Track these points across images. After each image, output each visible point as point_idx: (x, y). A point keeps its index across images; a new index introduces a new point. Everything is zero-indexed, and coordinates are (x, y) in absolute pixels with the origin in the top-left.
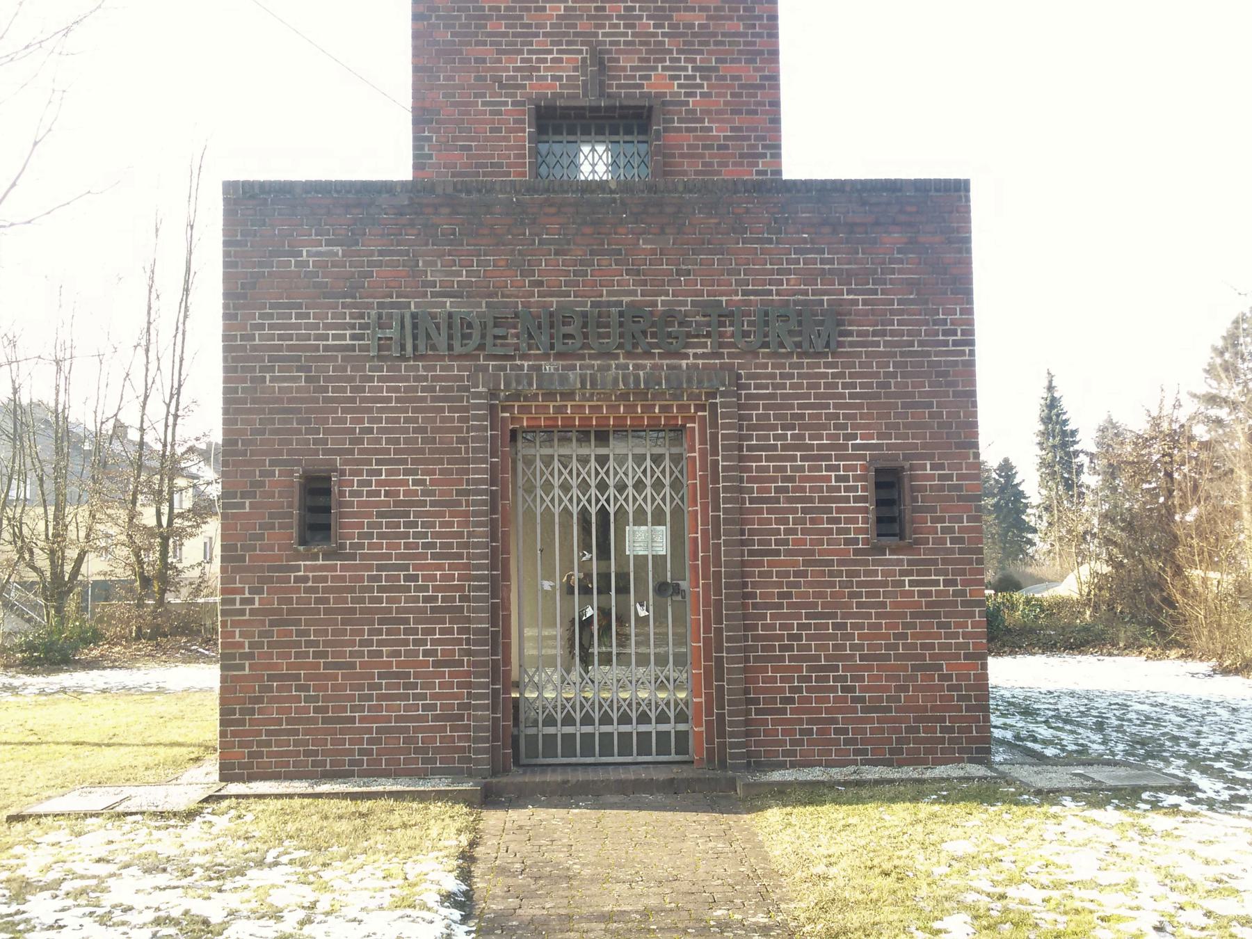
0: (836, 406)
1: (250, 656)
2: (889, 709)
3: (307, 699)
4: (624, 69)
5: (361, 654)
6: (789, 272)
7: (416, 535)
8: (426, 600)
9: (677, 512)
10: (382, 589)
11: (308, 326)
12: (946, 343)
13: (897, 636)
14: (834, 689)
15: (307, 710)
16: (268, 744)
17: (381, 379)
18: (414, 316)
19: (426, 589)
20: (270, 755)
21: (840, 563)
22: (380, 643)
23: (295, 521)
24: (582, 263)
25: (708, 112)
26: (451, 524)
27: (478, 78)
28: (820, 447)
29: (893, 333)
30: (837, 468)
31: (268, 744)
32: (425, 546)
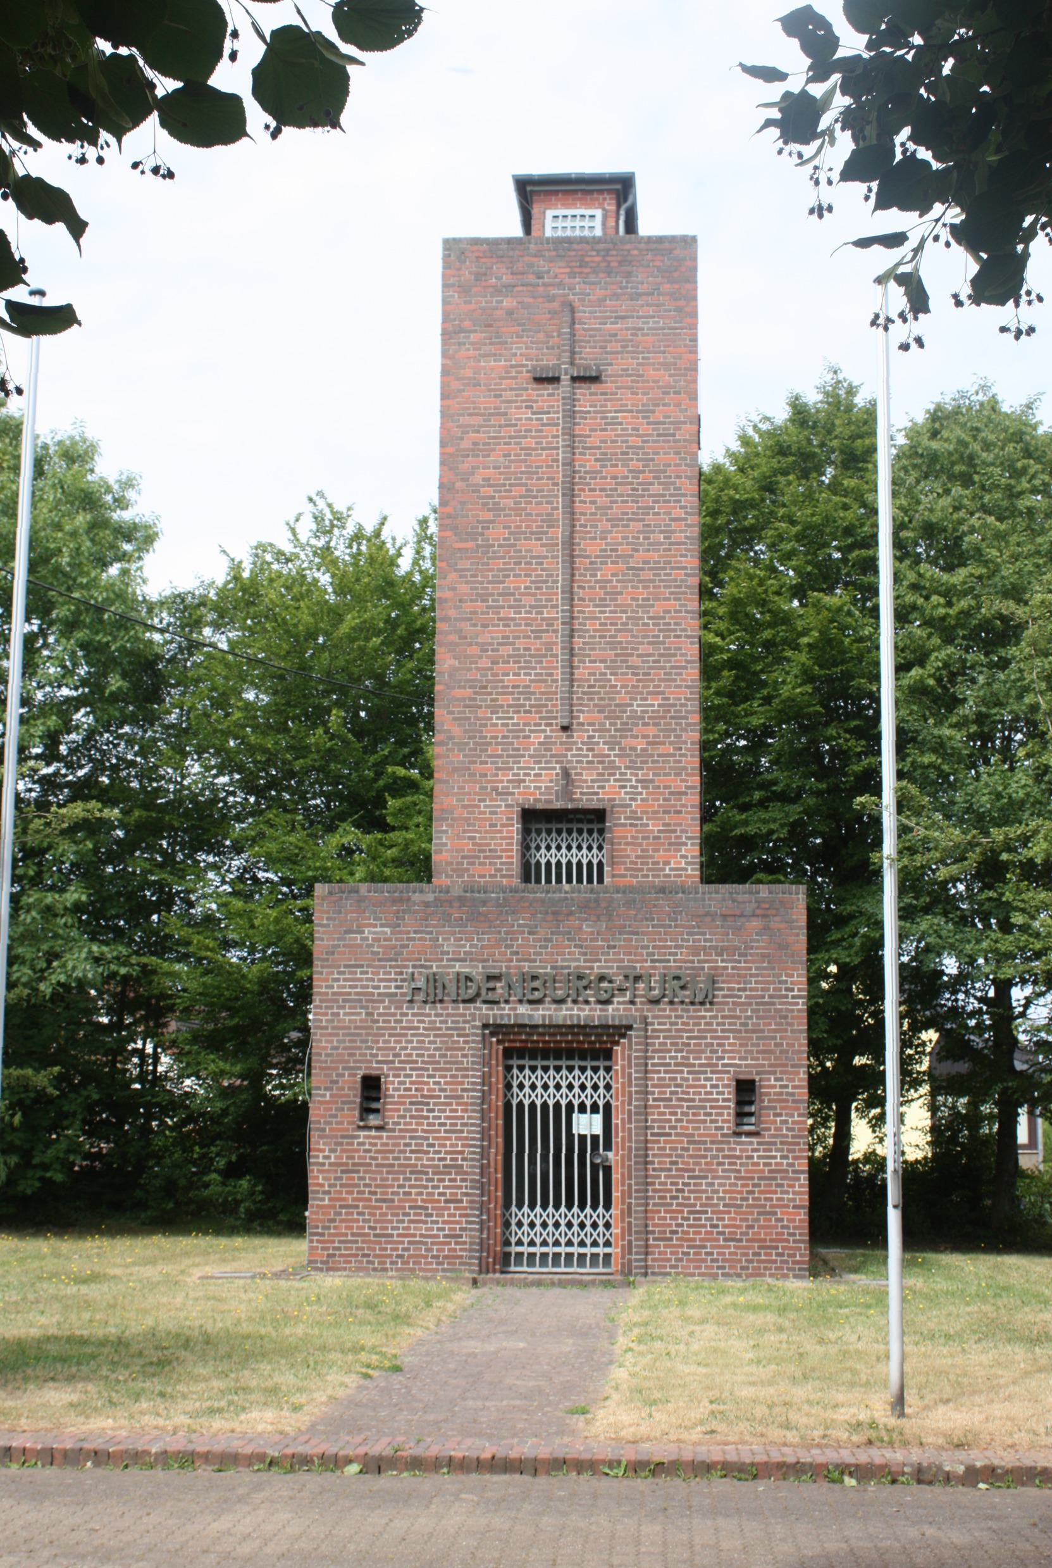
0: (712, 1038)
1: (329, 1192)
2: (740, 1240)
3: (364, 1221)
4: (586, 781)
5: (398, 1193)
6: (681, 947)
7: (435, 1118)
8: (440, 1159)
9: (607, 1106)
10: (412, 1152)
11: (368, 979)
12: (786, 996)
13: (748, 1192)
14: (705, 1226)
15: (363, 1228)
16: (339, 1249)
17: (414, 1015)
18: (434, 974)
19: (439, 1152)
20: (341, 1256)
21: (712, 1142)
22: (411, 1186)
23: (357, 1106)
24: (546, 940)
25: (646, 812)
26: (456, 1111)
27: (482, 788)
28: (700, 1065)
29: (751, 989)
30: (711, 1079)
31: (339, 1249)
32: (441, 1124)
